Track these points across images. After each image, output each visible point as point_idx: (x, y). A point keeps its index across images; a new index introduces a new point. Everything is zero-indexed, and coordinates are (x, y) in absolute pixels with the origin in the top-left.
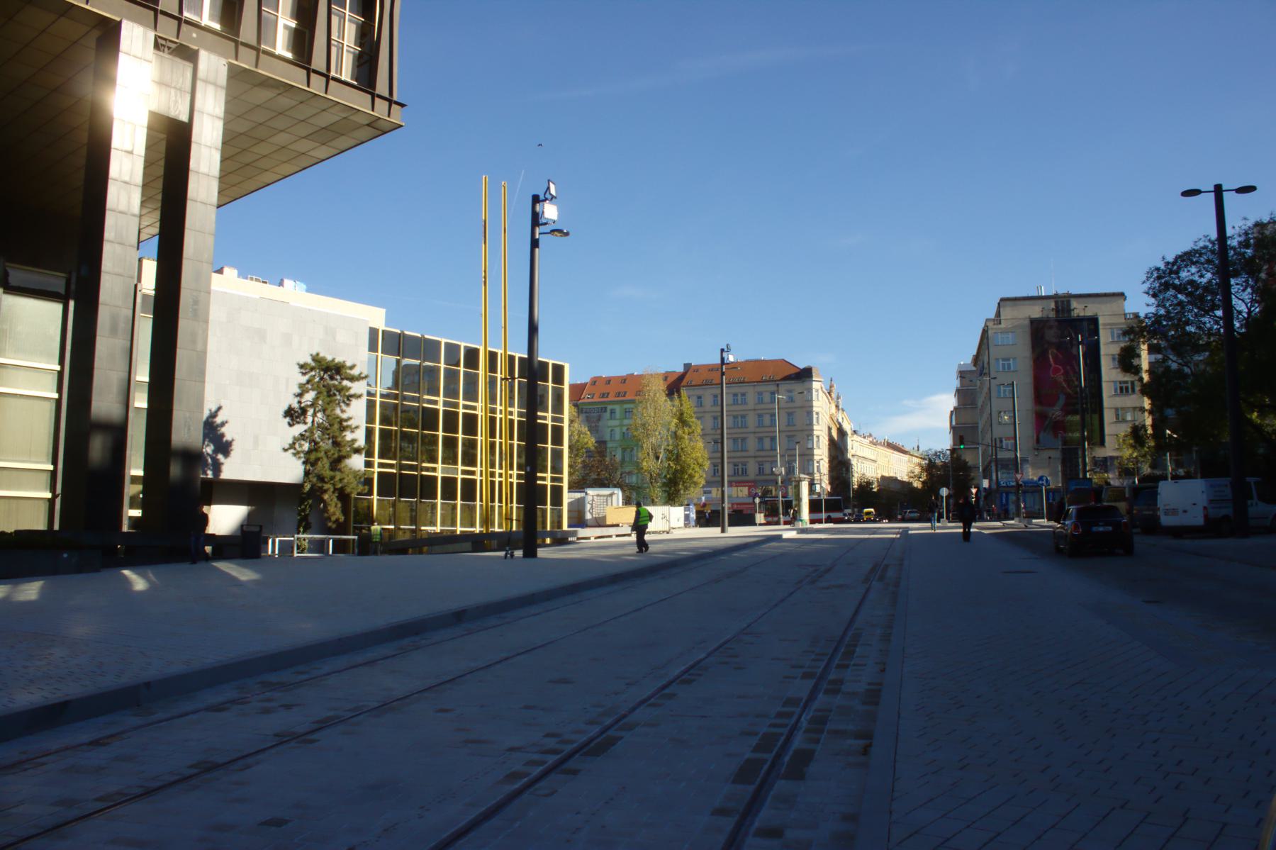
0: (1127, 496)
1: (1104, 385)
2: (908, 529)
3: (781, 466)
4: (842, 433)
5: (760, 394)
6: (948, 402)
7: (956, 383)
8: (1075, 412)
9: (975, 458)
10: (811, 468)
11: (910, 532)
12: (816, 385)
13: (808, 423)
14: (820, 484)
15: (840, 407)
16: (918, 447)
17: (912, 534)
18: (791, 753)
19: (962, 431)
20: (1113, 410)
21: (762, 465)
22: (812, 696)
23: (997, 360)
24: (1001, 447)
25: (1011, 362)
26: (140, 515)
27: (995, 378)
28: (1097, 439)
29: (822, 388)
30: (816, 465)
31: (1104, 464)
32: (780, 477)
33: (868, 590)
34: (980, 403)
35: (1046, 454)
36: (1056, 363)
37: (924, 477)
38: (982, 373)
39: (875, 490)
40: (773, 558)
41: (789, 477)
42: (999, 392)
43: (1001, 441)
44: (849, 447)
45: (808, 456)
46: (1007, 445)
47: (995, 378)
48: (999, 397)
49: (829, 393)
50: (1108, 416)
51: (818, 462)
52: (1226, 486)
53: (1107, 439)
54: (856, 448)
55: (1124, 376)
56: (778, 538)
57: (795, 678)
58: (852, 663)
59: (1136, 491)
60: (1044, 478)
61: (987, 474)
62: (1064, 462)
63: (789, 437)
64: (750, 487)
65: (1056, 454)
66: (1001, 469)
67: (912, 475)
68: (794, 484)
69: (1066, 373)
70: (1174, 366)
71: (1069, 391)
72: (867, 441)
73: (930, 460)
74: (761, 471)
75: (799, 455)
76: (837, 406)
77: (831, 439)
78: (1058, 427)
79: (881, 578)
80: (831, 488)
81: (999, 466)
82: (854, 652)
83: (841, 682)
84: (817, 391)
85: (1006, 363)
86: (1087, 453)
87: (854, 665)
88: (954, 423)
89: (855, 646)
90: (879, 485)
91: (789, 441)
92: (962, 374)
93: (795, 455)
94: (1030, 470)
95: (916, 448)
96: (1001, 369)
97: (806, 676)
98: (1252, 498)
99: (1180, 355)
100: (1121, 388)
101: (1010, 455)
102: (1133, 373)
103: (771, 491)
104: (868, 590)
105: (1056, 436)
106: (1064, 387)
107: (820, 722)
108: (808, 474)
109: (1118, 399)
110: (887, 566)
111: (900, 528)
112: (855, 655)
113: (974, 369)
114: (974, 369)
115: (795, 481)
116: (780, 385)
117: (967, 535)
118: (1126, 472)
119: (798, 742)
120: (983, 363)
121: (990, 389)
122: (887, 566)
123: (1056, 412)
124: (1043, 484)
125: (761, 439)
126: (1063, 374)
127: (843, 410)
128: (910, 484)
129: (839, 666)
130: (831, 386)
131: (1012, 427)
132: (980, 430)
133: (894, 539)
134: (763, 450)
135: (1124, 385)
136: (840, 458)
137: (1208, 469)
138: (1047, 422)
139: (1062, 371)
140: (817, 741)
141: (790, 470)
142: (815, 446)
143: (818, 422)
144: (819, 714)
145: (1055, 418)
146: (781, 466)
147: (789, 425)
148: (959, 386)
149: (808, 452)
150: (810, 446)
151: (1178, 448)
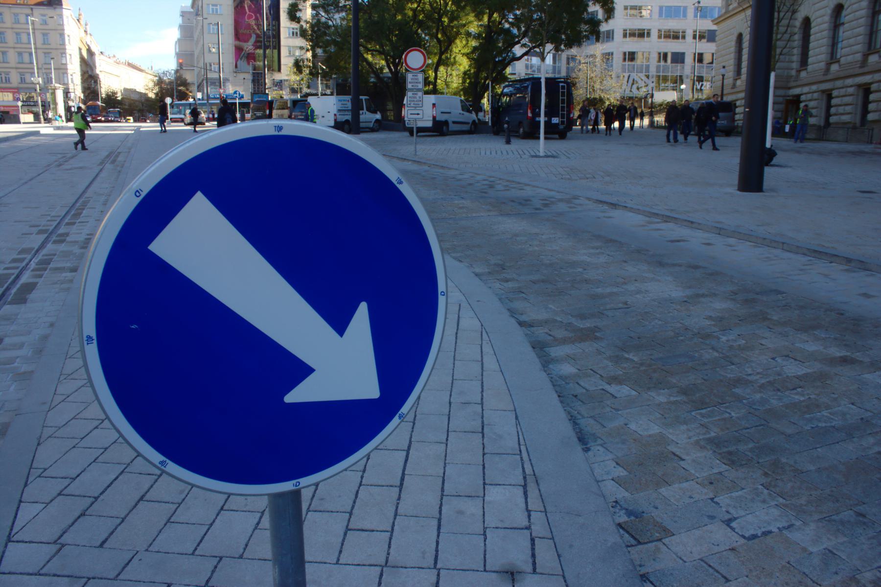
0: (289, 105)
1: (282, 30)
2: (141, 127)
3: (39, 77)
4: (90, 53)
5: (16, 15)
6: (174, 34)
7: (179, 20)
8: (259, 47)
9: (189, 77)
10: (66, 79)
11: (141, 129)
12: (66, 13)
13: (61, 43)
14: (74, 92)
15: (88, 32)
16: (152, 67)
17: (142, 131)
18: (18, 286)
19: (185, 58)
20: (287, 48)
21: (8, 74)
22: (43, 246)
23: (208, 5)
24: (211, 70)
25: (218, 7)
26: (553, 119)
27: (206, 19)
28: (276, 67)
29: (71, 15)
30: (70, 77)
31: (279, 84)
32: (38, 86)
33: (101, 170)
34: (196, 37)
35: (242, 76)
36: (249, 12)
37: (156, 90)
38: (197, 15)
39: (119, 98)
40: (30, 148)
41: (46, 86)
42: (209, 29)
43: (211, 65)
44: (97, 64)
45: (62, 70)
46: (215, 68)
47: (206, 19)
48: (209, 33)
49: (78, 20)
50: (284, 52)
51: (71, 75)
52: (348, 101)
53: (282, 67)
54: (102, 67)
55: (291, 24)
56: (37, 133)
57: (32, 234)
58: (78, 221)
59: (295, 102)
60: (238, 93)
61: (200, 88)
62: (253, 81)
63: (45, 53)
64: (14, 93)
65: (249, 77)
66: (211, 85)
67: (147, 88)
68: (50, 91)
69: (257, 19)
70: (323, 20)
71: (258, 32)
72: (112, 61)
73: (160, 78)
74: (23, 80)
75: (55, 69)
76: (86, 32)
77: (82, 59)
78: (250, 57)
79: (113, 162)
80: (84, 96)
81: (209, 83)
82: (81, 213)
83: (67, 234)
84: (67, 17)
85: (215, 8)
86: (266, 76)
87: (79, 222)
88: (177, 50)
89: (84, 209)
90: (122, 95)
91: (45, 57)
92: (183, 14)
93: (51, 69)
94: (230, 87)
95: (150, 68)
96: (211, 12)
97: (40, 232)
98: (363, 109)
99: (326, 12)
100: (293, 33)
101: (216, 76)
102: (296, 22)
103: (33, 97)
104: (101, 170)
105: (249, 64)
106: (254, 29)
107: (45, 263)
108: (64, 84)
109: (290, 40)
110: (119, 153)
111: (135, 127)
112: (82, 215)
113: (192, 10)
114: (192, 10)
115: (52, 89)
116: (34, 10)
117: (195, 131)
118: (293, 91)
119: (24, 279)
120: (198, 6)
121: (203, 26)
122: (119, 153)
123: (249, 46)
124: (236, 97)
125: (20, 54)
126: (254, 20)
127: (91, 35)
128: (146, 94)
129: (68, 224)
130: (80, 15)
131: (218, 55)
132: (196, 56)
133: (129, 134)
134: (23, 63)
135: (295, 31)
136: (90, 73)
137: (341, 90)
138: (243, 53)
139: (254, 17)
140: (41, 276)
141: (48, 80)
142: (68, 62)
143: (69, 43)
144: (46, 257)
145: (249, 51)
146: (39, 77)
147: (44, 44)
148: (181, 22)
149: (63, 67)
150: (64, 62)
151: (325, 76)
